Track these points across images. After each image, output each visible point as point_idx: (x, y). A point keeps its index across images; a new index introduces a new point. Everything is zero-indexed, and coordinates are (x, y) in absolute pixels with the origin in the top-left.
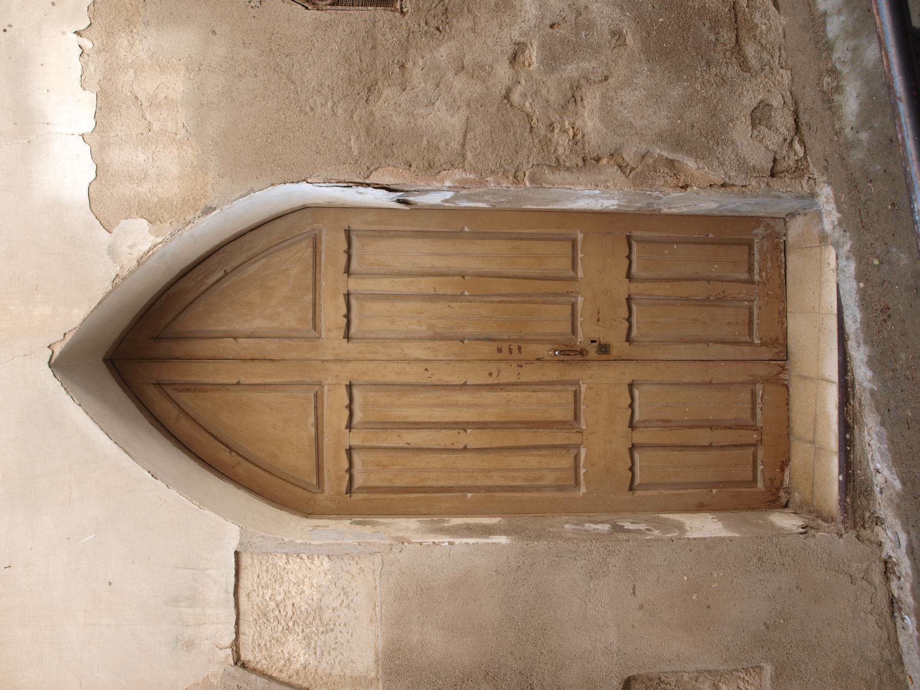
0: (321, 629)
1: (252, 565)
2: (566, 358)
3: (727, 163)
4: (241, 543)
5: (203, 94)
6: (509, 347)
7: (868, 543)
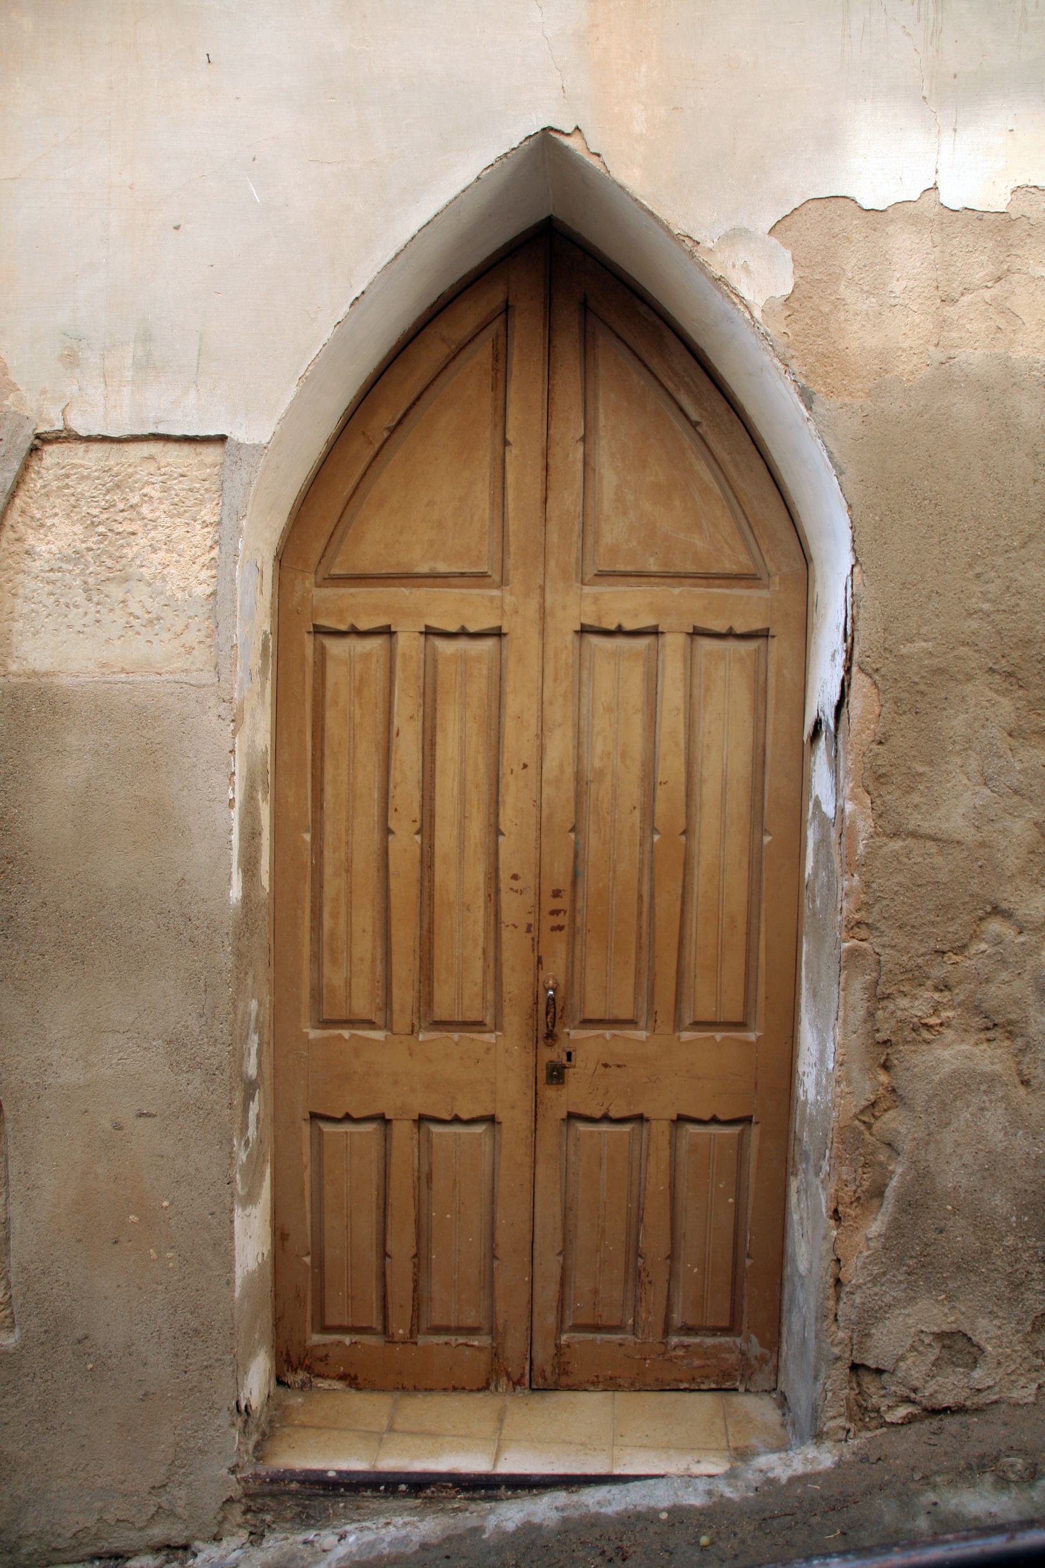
0: (91, 580)
1: (203, 465)
2: (542, 1007)
3: (876, 1289)
4: (239, 446)
5: (1004, 391)
6: (561, 910)
7: (220, 1517)
